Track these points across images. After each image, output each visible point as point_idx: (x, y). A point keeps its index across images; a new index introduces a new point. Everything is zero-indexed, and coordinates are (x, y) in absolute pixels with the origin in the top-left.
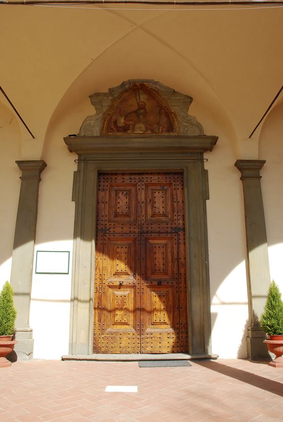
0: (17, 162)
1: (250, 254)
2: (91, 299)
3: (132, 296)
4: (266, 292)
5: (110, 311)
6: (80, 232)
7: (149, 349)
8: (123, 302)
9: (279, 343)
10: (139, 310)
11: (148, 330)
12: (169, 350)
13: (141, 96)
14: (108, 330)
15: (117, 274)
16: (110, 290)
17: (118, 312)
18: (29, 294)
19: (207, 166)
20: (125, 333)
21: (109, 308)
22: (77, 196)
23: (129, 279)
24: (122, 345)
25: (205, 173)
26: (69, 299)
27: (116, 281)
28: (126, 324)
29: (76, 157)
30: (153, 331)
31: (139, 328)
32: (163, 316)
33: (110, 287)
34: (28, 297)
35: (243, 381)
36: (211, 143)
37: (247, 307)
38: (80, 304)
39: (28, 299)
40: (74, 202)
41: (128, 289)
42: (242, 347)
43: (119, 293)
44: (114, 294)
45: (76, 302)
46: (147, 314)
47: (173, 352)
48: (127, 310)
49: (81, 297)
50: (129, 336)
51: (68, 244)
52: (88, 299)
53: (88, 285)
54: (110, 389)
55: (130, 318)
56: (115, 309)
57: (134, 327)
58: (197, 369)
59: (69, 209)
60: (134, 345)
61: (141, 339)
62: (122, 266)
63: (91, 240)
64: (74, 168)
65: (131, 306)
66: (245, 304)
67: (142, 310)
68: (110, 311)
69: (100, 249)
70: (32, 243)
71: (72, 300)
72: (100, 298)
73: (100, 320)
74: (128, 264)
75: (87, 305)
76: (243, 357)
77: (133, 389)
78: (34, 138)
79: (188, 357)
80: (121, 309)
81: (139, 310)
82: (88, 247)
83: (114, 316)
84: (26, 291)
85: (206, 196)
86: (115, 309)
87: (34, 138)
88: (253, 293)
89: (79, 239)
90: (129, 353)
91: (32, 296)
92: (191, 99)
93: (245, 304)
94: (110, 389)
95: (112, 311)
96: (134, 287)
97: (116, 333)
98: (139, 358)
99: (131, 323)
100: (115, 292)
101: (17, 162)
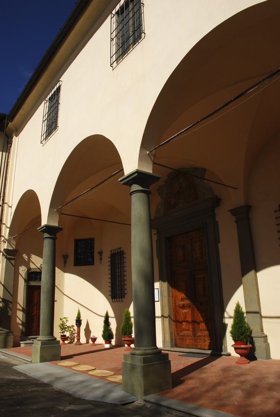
0: (229, 211)
3: (190, 313)
4: (104, 314)
7: (199, 346)
12: (207, 348)
14: (181, 334)
15: (182, 299)
17: (184, 323)
19: (218, 219)
20: (187, 336)
23: (187, 302)
25: (216, 225)
28: (188, 330)
32: (203, 326)
34: (258, 315)
39: (259, 319)
46: (197, 324)
48: (188, 322)
50: (190, 338)
56: (183, 321)
62: (183, 295)
65: (190, 319)
70: (253, 272)
73: (176, 328)
74: (186, 294)
80: (185, 321)
85: (217, 241)
86: (183, 321)
95: (181, 322)
97: (184, 335)
98: (179, 350)
101: (229, 211)
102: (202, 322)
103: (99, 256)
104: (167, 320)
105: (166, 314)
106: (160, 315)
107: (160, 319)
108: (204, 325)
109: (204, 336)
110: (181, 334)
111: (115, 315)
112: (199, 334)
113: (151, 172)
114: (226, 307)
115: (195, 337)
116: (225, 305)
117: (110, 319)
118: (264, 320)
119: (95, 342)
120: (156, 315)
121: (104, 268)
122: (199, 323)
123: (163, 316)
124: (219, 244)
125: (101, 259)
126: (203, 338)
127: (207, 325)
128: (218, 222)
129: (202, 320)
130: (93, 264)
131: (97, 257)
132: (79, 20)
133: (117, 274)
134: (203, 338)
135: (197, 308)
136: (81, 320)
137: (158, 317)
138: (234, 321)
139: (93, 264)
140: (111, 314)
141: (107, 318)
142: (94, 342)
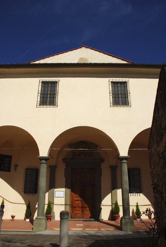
2: (70, 204)
4: (136, 205)
5: (75, 207)
6: (66, 187)
7: (85, 217)
8: (78, 205)
10: (83, 207)
11: (85, 212)
12: (89, 218)
14: (75, 212)
15: (77, 197)
16: (75, 202)
18: (54, 203)
19: (101, 167)
20: (79, 213)
21: (75, 206)
22: (66, 176)
23: (79, 198)
24: (78, 216)
25: (101, 169)
26: (64, 204)
27: (77, 199)
28: (80, 211)
29: (65, 164)
30: (86, 212)
31: (83, 212)
32: (88, 209)
33: (75, 201)
36: (103, 160)
37: (111, 207)
38: (67, 206)
40: (64, 178)
41: (113, 227)
42: (40, 183)
43: (77, 202)
44: (76, 202)
45: (66, 205)
47: (90, 218)
48: (79, 207)
49: (67, 204)
51: (64, 189)
52: (69, 204)
53: (69, 201)
54: (77, 225)
55: (80, 209)
57: (81, 212)
58: (96, 223)
59: (64, 179)
63: (70, 189)
64: (65, 167)
65: (80, 206)
66: (131, 206)
68: (75, 207)
69: (72, 191)
71: (65, 205)
72: (72, 203)
73: (72, 210)
74: (79, 195)
75: (69, 206)
77: (82, 225)
79: (94, 219)
80: (78, 207)
81: (83, 207)
82: (69, 191)
83: (76, 209)
84: (53, 202)
85: (101, 176)
89: (66, 188)
91: (54, 204)
92: (98, 146)
93: (131, 206)
94: (77, 225)
96: (81, 200)
97: (77, 213)
98: (20, 232)
99: (80, 210)
103: (15, 168)
105: (68, 203)
110: (75, 212)
112: (85, 212)
114: (102, 201)
115: (83, 213)
116: (102, 200)
117: (139, 207)
118: (54, 205)
119: (14, 219)
120: (122, 207)
121: (20, 176)
122: (86, 208)
124: (101, 177)
127: (89, 208)
130: (9, 171)
131: (12, 168)
133: (34, 179)
135: (85, 202)
136: (4, 205)
139: (9, 171)
142: (13, 218)
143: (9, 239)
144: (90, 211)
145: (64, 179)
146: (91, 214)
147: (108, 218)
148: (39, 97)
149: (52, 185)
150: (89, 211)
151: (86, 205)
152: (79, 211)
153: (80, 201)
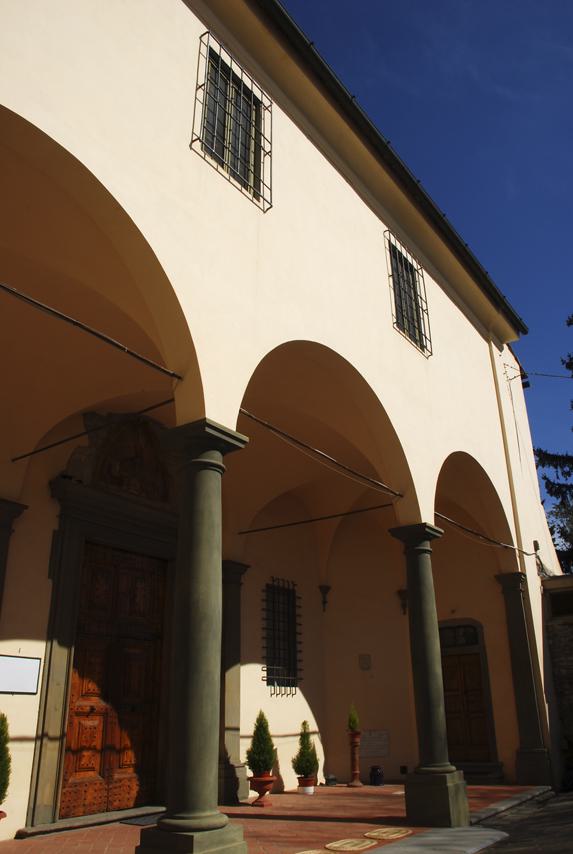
1: (227, 674)
3: (101, 728)
4: (299, 730)
9: (321, 748)
11: (116, 776)
12: (132, 803)
13: (204, 823)
17: (85, 753)
18: (238, 729)
22: (55, 572)
23: (96, 702)
24: (87, 802)
28: (93, 769)
32: (130, 757)
35: (306, 135)
40: (50, 582)
47: (137, 805)
49: (51, 733)
50: (96, 787)
51: (38, 648)
56: (84, 748)
60: (100, 801)
61: (108, 790)
65: (98, 743)
67: (112, 748)
76: (192, 837)
78: (13, 460)
80: (89, 749)
87: (13, 460)
88: (227, 725)
90: (92, 813)
97: (80, 784)
99: (97, 767)
100: (83, 722)
102: (128, 749)
104: (52, 750)
105: (54, 730)
106: (57, 733)
107: (56, 744)
108: (133, 755)
109: (130, 780)
111: (319, 728)
113: (235, 430)
115: (108, 783)
122: (121, 751)
123: (41, 737)
125: (324, 602)
126: (129, 783)
128: (13, 531)
129: (128, 743)
132: (348, 124)
134: (129, 783)
137: (314, 733)
138: (254, 744)
140: (313, 726)
141: (304, 737)
143: (258, 843)
144: (138, 768)
145: (46, 586)
146: (140, 786)
147: (285, 784)
148: (200, 107)
149: (232, 657)
150: (131, 770)
151: (125, 735)
152: (91, 773)
153: (99, 714)
